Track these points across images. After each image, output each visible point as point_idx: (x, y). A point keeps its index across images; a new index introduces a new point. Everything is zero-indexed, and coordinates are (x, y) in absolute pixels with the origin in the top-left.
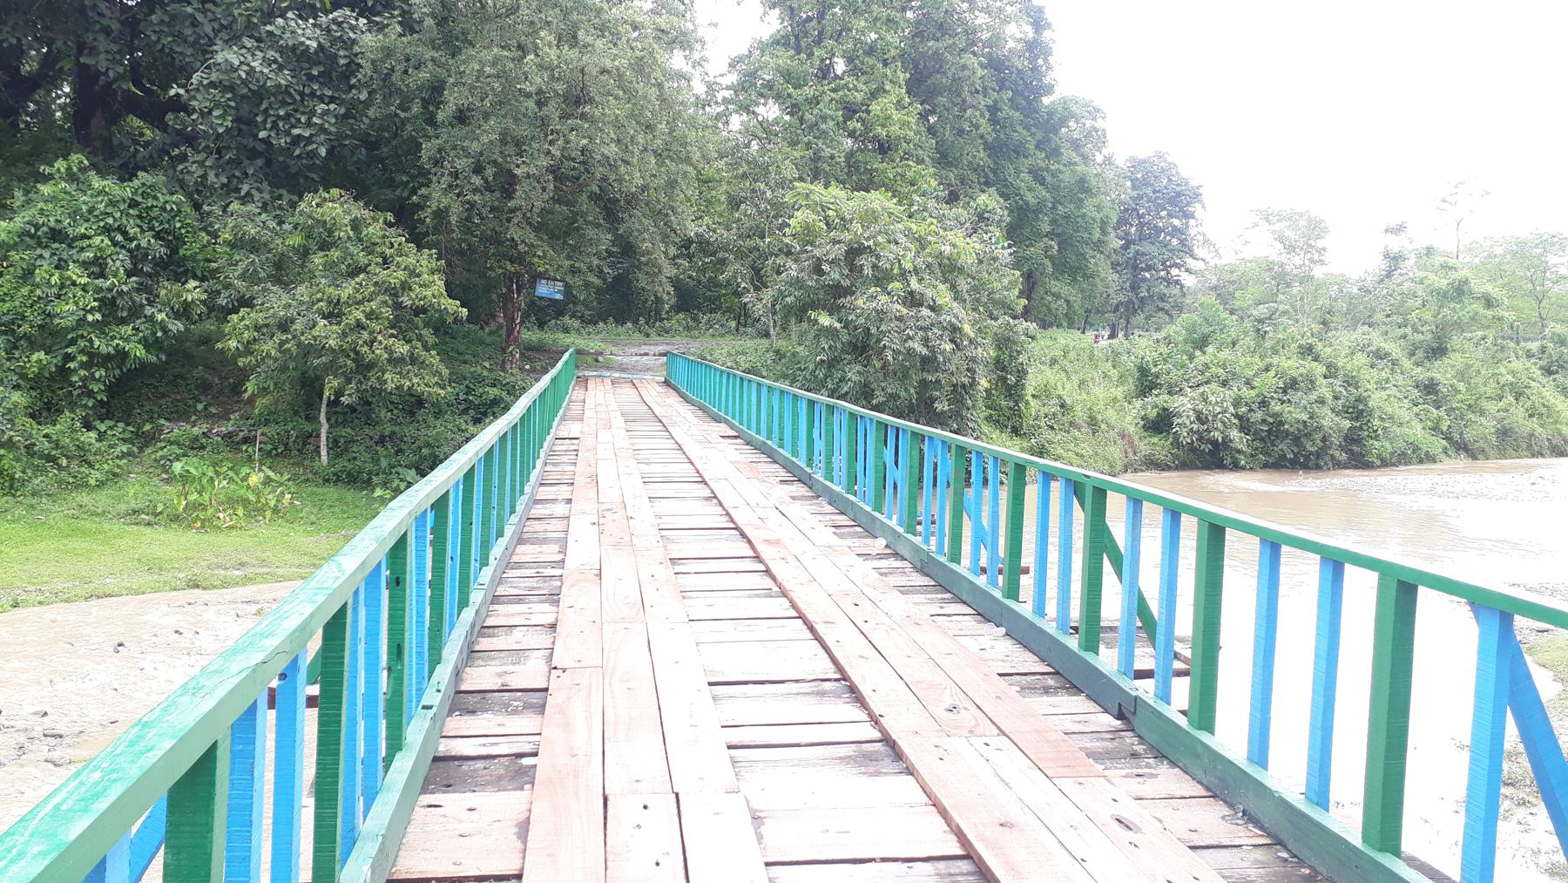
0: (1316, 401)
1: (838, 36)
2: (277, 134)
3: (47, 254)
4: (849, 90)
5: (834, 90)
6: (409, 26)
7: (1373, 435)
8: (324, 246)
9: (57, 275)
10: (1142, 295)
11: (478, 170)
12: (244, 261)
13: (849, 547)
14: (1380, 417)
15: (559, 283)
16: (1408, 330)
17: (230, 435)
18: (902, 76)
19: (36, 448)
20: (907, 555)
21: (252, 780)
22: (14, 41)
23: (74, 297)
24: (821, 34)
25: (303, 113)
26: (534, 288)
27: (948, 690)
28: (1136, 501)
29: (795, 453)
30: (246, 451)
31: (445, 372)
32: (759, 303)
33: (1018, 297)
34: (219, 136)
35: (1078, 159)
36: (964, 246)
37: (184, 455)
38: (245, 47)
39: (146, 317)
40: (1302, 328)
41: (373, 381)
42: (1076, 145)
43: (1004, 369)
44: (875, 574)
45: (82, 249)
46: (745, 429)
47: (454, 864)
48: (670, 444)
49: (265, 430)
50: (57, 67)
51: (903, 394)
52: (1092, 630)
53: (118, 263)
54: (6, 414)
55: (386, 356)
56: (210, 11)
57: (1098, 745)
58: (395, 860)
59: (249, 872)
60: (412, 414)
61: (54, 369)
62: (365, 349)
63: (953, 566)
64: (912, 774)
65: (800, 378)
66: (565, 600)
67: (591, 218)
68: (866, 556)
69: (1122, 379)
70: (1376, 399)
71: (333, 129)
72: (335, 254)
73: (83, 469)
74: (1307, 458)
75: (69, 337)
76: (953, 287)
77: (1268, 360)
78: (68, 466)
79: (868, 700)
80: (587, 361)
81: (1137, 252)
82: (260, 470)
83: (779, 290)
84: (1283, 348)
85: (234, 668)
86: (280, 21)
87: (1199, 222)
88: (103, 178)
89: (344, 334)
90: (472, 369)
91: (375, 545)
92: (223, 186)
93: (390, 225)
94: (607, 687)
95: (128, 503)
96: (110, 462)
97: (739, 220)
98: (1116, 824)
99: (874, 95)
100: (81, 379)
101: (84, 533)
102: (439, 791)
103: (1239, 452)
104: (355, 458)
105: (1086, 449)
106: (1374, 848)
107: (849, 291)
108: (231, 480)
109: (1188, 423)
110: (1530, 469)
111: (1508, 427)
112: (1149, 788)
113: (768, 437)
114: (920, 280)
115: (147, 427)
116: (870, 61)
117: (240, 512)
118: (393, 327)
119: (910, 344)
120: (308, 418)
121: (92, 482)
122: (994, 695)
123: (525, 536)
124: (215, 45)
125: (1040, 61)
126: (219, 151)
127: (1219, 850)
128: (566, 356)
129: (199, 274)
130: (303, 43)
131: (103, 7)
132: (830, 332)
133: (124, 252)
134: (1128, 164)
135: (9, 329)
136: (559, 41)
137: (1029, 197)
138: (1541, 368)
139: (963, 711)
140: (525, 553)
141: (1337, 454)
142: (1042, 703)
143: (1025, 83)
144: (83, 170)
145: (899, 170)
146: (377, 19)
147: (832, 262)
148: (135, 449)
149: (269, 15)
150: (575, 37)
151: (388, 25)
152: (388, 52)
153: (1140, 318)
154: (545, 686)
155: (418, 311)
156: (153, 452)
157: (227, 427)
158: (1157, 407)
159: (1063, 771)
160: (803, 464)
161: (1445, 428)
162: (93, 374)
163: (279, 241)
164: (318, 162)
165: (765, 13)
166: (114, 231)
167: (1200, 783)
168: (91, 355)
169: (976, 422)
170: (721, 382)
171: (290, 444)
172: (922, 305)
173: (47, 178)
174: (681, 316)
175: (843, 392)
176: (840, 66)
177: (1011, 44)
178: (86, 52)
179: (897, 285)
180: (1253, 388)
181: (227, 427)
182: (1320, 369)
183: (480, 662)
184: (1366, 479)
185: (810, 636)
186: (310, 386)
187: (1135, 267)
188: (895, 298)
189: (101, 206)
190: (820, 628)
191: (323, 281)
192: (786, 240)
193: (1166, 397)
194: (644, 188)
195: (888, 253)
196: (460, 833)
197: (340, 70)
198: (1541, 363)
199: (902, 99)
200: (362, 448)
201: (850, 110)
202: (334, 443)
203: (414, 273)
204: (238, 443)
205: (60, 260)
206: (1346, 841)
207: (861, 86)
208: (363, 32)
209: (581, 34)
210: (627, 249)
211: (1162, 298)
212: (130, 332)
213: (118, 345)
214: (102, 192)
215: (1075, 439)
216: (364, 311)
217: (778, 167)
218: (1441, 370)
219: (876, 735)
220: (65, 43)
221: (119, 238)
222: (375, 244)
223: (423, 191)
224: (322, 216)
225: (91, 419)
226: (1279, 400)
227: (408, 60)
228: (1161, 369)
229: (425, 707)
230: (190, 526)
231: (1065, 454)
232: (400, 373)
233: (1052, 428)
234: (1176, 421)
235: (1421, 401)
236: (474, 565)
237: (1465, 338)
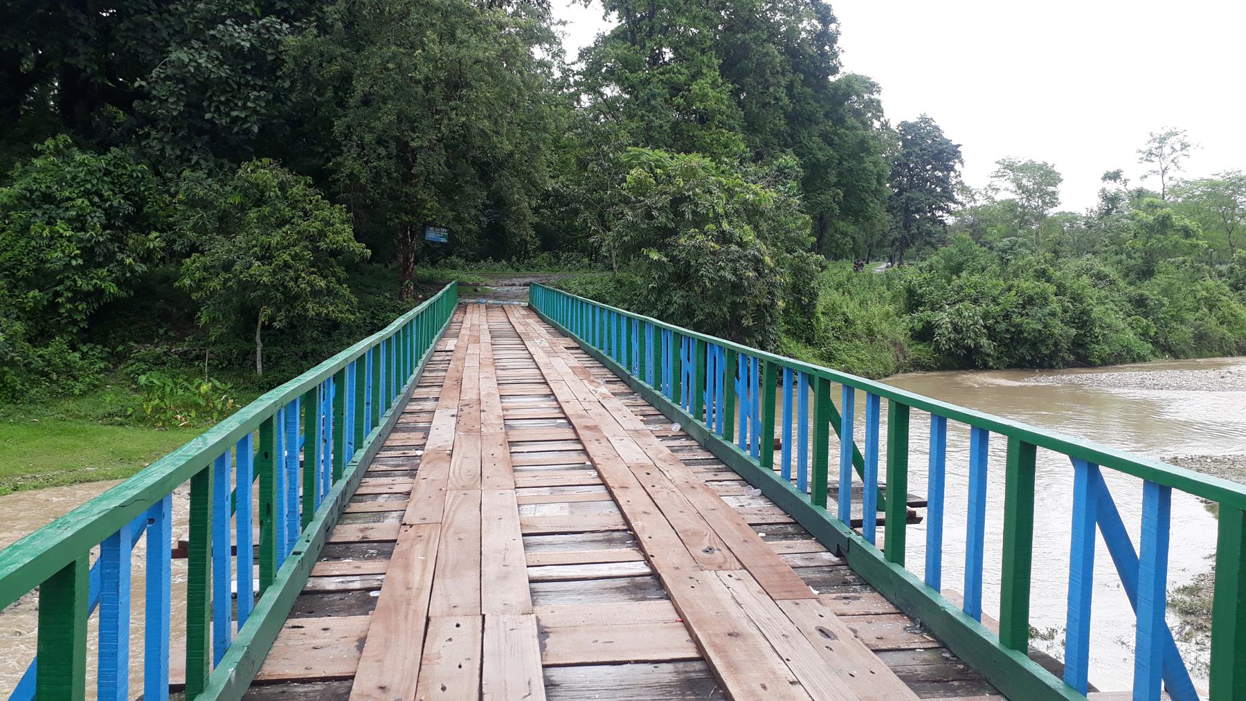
1: (664, 31)
2: (219, 116)
3: (39, 213)
4: (674, 73)
5: (662, 74)
6: (323, 28)
7: (1094, 340)
8: (259, 202)
9: (47, 230)
10: (913, 232)
11: (380, 142)
12: (197, 215)
13: (652, 431)
14: (1100, 326)
15: (444, 230)
16: (1124, 257)
18: (716, 62)
19: (32, 366)
20: (695, 436)
21: (118, 595)
22: (12, 46)
23: (62, 246)
24: (652, 28)
26: (424, 234)
27: (708, 537)
28: (850, 388)
29: (619, 359)
31: (354, 300)
32: (607, 241)
33: (810, 235)
34: (174, 118)
35: (858, 124)
36: (769, 196)
37: (149, 370)
38: (193, 48)
39: (117, 261)
40: (1036, 258)
41: (298, 310)
42: (858, 114)
43: (799, 292)
45: (67, 209)
47: (306, 669)
49: (212, 349)
50: (48, 66)
51: (717, 312)
52: (822, 491)
53: (96, 219)
54: (9, 339)
55: (309, 289)
57: (817, 576)
58: (261, 666)
60: (330, 335)
62: (292, 284)
64: (670, 599)
66: (421, 473)
68: (664, 438)
69: (894, 299)
70: (1097, 311)
71: (263, 111)
72: (266, 210)
73: (69, 382)
74: (1042, 360)
76: (756, 228)
78: (58, 380)
79: (644, 544)
80: (467, 294)
81: (908, 198)
82: (209, 381)
83: (619, 231)
85: (95, 511)
86: (221, 27)
87: (957, 173)
89: (274, 273)
90: (376, 298)
92: (177, 157)
93: (310, 186)
94: (442, 537)
95: (105, 407)
96: (91, 376)
97: (588, 178)
98: (818, 634)
99: (694, 77)
100: (67, 311)
101: (70, 433)
103: (988, 355)
104: (284, 370)
105: (865, 354)
106: (1007, 647)
107: (674, 232)
108: (187, 389)
109: (947, 333)
110: (1219, 366)
111: (1203, 332)
114: (730, 223)
115: (120, 348)
116: (691, 50)
117: (193, 414)
118: (312, 267)
119: (722, 273)
120: (246, 339)
121: (77, 392)
122: (742, 540)
123: (398, 426)
124: (170, 46)
125: (827, 48)
127: (897, 652)
128: (448, 286)
129: (159, 226)
130: (239, 44)
132: (658, 264)
133: (100, 210)
134: (900, 128)
135: (10, 271)
136: (441, 39)
137: (820, 155)
138: (1230, 285)
139: (716, 552)
140: (397, 439)
142: (779, 546)
144: (68, 147)
145: (715, 136)
147: (659, 210)
148: (111, 366)
149: (213, 21)
150: (453, 35)
152: (306, 50)
153: (912, 250)
155: (334, 253)
156: (124, 368)
157: (183, 347)
158: (922, 321)
159: (785, 595)
160: (624, 368)
161: (1152, 334)
165: (607, 14)
166: (92, 194)
167: (892, 603)
168: (75, 292)
170: (567, 305)
171: (233, 360)
173: (37, 154)
174: (545, 254)
175: (671, 312)
176: (668, 54)
177: (804, 35)
178: (69, 53)
180: (998, 304)
181: (183, 347)
182: (1051, 289)
183: (349, 521)
184: (1089, 375)
185: (608, 497)
186: (248, 314)
187: (907, 210)
189: (82, 175)
190: (616, 492)
191: (257, 231)
193: (929, 313)
194: (511, 154)
195: (705, 201)
196: (313, 646)
197: (268, 65)
198: (1230, 281)
199: (716, 80)
200: (289, 362)
201: (675, 89)
202: (267, 359)
203: (328, 223)
204: (192, 360)
205: (50, 217)
207: (684, 70)
208: (286, 35)
209: (459, 33)
210: (499, 202)
211: (929, 234)
212: (105, 274)
213: (96, 284)
214: (82, 164)
216: (290, 254)
218: (1150, 290)
219: (647, 570)
221: (96, 199)
222: (297, 201)
223: (339, 159)
225: (76, 343)
227: (322, 55)
228: (925, 291)
229: (295, 553)
230: (153, 426)
232: (319, 303)
233: (838, 338)
234: (937, 331)
235: (1134, 313)
236: (347, 447)
237: (1169, 262)
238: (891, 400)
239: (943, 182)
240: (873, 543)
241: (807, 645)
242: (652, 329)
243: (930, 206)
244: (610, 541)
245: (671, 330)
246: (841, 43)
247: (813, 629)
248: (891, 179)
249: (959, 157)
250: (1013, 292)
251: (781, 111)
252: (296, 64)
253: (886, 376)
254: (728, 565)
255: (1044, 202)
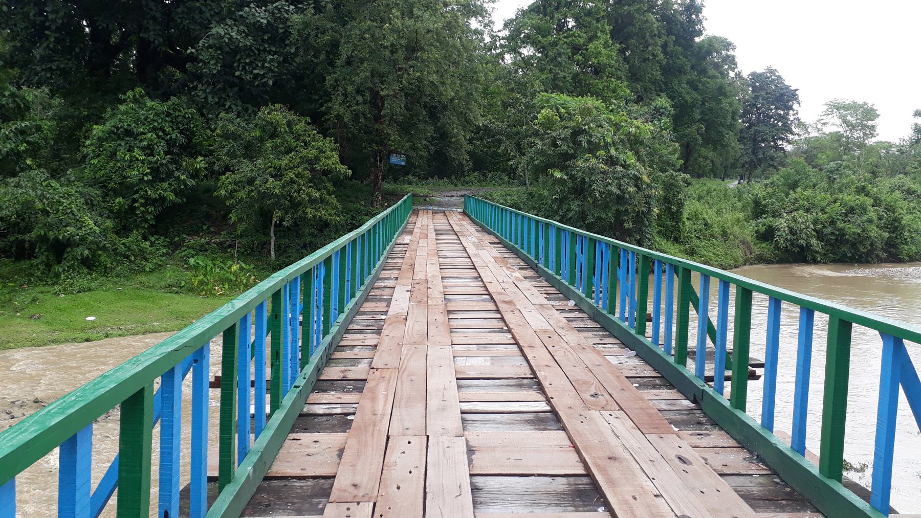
0: (866, 221)
2: (245, 73)
3: (123, 144)
4: (575, 37)
5: (566, 37)
6: (319, 9)
7: (904, 242)
8: (273, 136)
9: (128, 155)
11: (359, 91)
12: (230, 145)
15: (403, 156)
17: (221, 243)
18: (607, 28)
19: (118, 251)
25: (260, 61)
28: (706, 276)
29: (529, 252)
30: (230, 252)
33: (678, 159)
34: (214, 75)
36: (647, 129)
38: (227, 25)
39: (175, 177)
41: (300, 213)
42: (717, 66)
43: (669, 202)
44: (565, 321)
45: (141, 140)
46: (504, 238)
47: (302, 469)
48: (460, 247)
49: (240, 240)
52: (683, 353)
53: (160, 148)
56: (209, 5)
57: (678, 417)
58: (271, 466)
59: (172, 460)
60: (322, 231)
61: (127, 207)
62: (296, 194)
63: (610, 316)
64: (564, 430)
65: (543, 210)
66: (385, 332)
67: (421, 118)
68: (562, 311)
69: (744, 208)
70: (906, 219)
71: (276, 70)
72: (278, 141)
73: (142, 262)
74: (860, 256)
75: (135, 189)
76: (637, 153)
77: (836, 196)
78: (135, 261)
79: (546, 389)
80: (419, 203)
81: (756, 131)
82: (238, 263)
84: (846, 188)
85: (158, 353)
88: (153, 101)
89: (284, 186)
90: (355, 206)
91: (257, 295)
92: (216, 103)
93: (309, 124)
94: (399, 378)
98: (677, 461)
99: (590, 40)
100: (141, 212)
101: (143, 298)
102: (300, 432)
103: (817, 252)
104: (290, 256)
105: (720, 251)
107: (573, 157)
109: (784, 235)
112: (705, 441)
113: (516, 243)
114: (616, 149)
116: (588, 19)
117: (227, 286)
119: (609, 187)
120: (264, 234)
121: (147, 269)
126: (214, 84)
128: (406, 197)
129: (203, 153)
130: (259, 21)
131: (152, 4)
132: (561, 181)
134: (750, 77)
137: (688, 98)
141: (880, 253)
142: (649, 394)
143: (685, 31)
144: (142, 96)
146: (300, 6)
147: (562, 140)
148: (170, 251)
149: (240, 7)
150: (412, 12)
151: (306, 9)
152: (306, 25)
154: (366, 378)
155: (326, 173)
156: (179, 253)
158: (765, 225)
159: (652, 430)
160: (533, 258)
162: (147, 210)
163: (247, 134)
164: (268, 89)
166: (158, 130)
167: (735, 439)
168: (146, 199)
169: (651, 234)
170: (492, 210)
172: (617, 164)
173: (122, 102)
174: (476, 174)
176: (571, 23)
179: (602, 152)
180: (826, 213)
182: (869, 201)
183: (334, 365)
185: (520, 354)
186: (265, 216)
187: (755, 140)
188: (601, 160)
190: (526, 350)
191: (272, 156)
192: (536, 127)
193: (771, 219)
194: (452, 100)
195: (597, 134)
199: (608, 41)
200: (294, 251)
201: (576, 49)
202: (278, 248)
204: (226, 248)
205: (130, 146)
206: (810, 472)
207: (583, 35)
208: (292, 14)
209: (415, 10)
210: (443, 136)
211: (772, 158)
212: (167, 186)
214: (152, 108)
215: (713, 245)
216: (294, 173)
217: (532, 84)
219: (548, 408)
220: (132, 26)
221: (161, 133)
223: (330, 104)
224: (271, 119)
226: (842, 220)
227: (317, 29)
229: (295, 387)
230: (199, 294)
231: (707, 254)
232: (315, 208)
233: (699, 238)
234: (777, 233)
236: (333, 312)
238: (738, 286)
239: (783, 118)
240: (722, 394)
241: (668, 469)
242: (555, 230)
243: (773, 137)
244: (521, 386)
245: (568, 231)
246: (705, 13)
247: (673, 457)
248: (742, 116)
249: (797, 99)
250: (838, 204)
251: (657, 64)
252: (299, 35)
253: (736, 267)
254: (609, 407)
255: (865, 134)
